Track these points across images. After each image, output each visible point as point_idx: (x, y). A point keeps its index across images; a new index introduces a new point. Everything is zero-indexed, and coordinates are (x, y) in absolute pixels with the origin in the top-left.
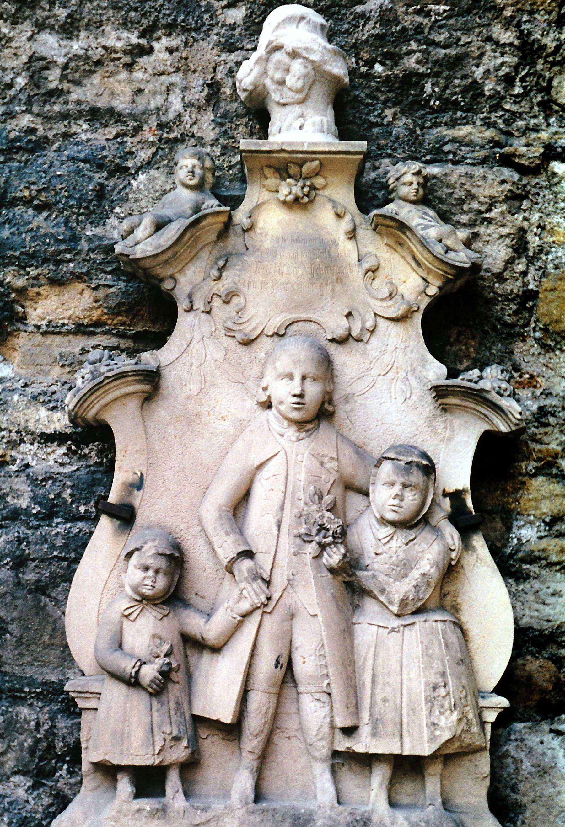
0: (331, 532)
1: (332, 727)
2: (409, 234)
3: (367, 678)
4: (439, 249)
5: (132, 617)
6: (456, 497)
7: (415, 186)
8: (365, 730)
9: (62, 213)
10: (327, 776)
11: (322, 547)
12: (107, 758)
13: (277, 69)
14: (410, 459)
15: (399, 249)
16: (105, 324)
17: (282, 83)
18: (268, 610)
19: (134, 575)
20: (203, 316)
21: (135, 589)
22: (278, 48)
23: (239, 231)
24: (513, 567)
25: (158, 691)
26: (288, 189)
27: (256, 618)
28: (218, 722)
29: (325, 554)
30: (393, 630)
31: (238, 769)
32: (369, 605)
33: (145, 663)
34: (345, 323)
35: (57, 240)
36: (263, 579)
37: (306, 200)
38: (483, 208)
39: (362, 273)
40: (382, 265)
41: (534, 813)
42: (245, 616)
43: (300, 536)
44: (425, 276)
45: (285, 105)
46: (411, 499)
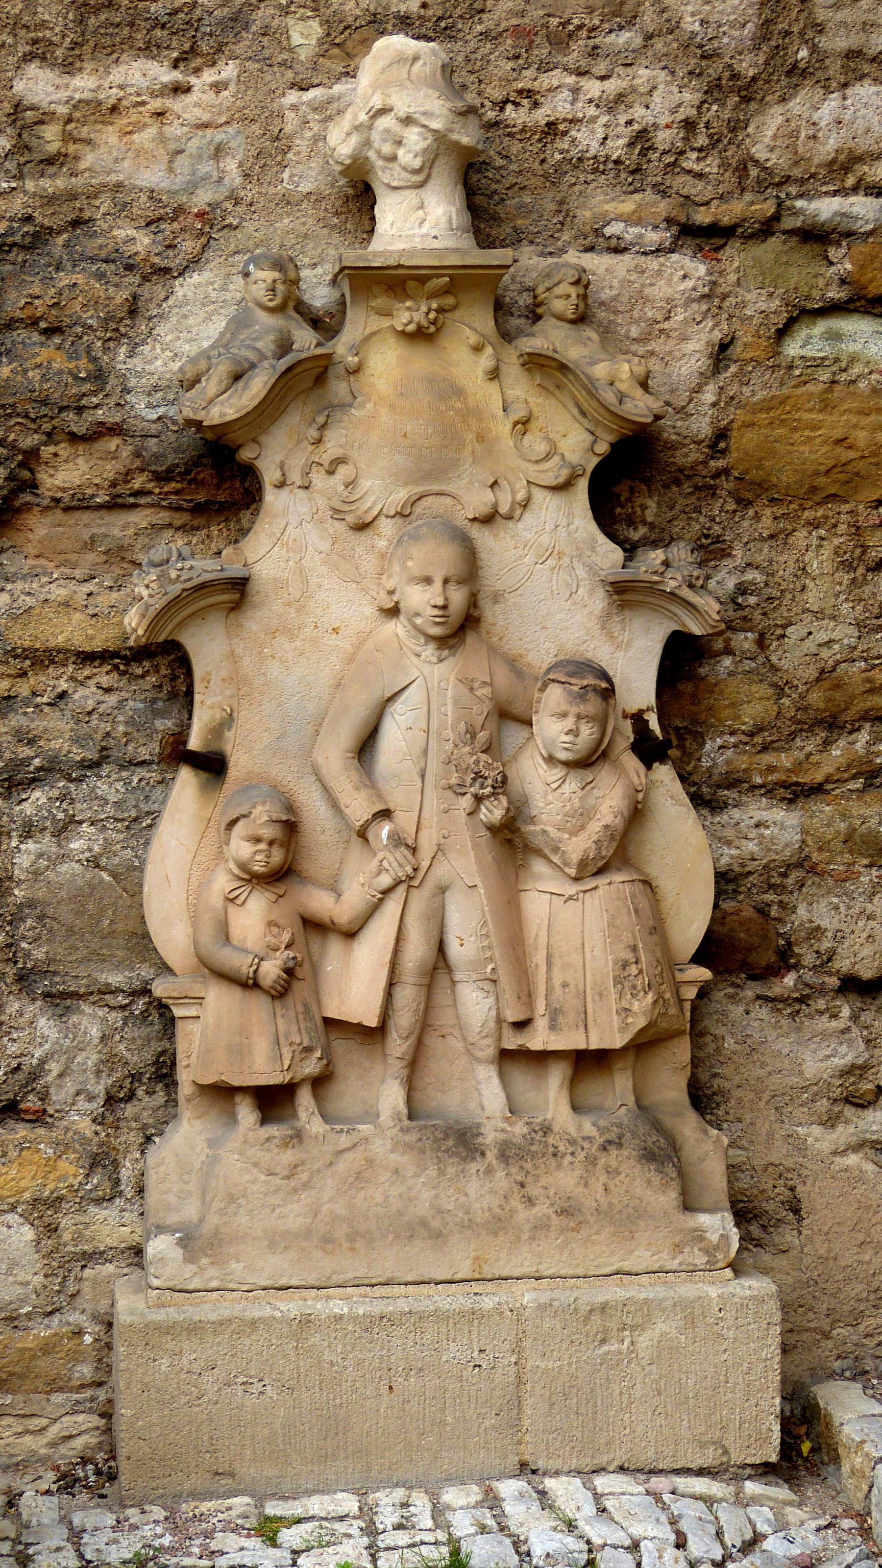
0: (490, 781)
1: (499, 1021)
2: (571, 377)
3: (539, 958)
4: (609, 397)
5: (239, 902)
6: (638, 719)
7: (574, 299)
8: (541, 1024)
9: (81, 338)
10: (496, 1080)
11: (479, 799)
12: (223, 1078)
13: (385, 140)
14: (585, 683)
15: (558, 393)
16: (150, 493)
17: (393, 158)
18: (416, 883)
19: (240, 848)
20: (301, 493)
21: (243, 866)
22: (384, 111)
23: (342, 372)
24: (705, 799)
25: (280, 993)
26: (408, 314)
27: (400, 893)
28: (360, 1025)
29: (484, 810)
30: (570, 898)
31: (383, 1081)
32: (539, 866)
33: (262, 959)
34: (488, 497)
35: (76, 378)
36: (407, 845)
37: (432, 329)
38: (659, 318)
39: (509, 426)
40: (535, 414)
41: (740, 1100)
42: (386, 892)
43: (450, 788)
44: (592, 428)
45: (396, 188)
46: (587, 733)
